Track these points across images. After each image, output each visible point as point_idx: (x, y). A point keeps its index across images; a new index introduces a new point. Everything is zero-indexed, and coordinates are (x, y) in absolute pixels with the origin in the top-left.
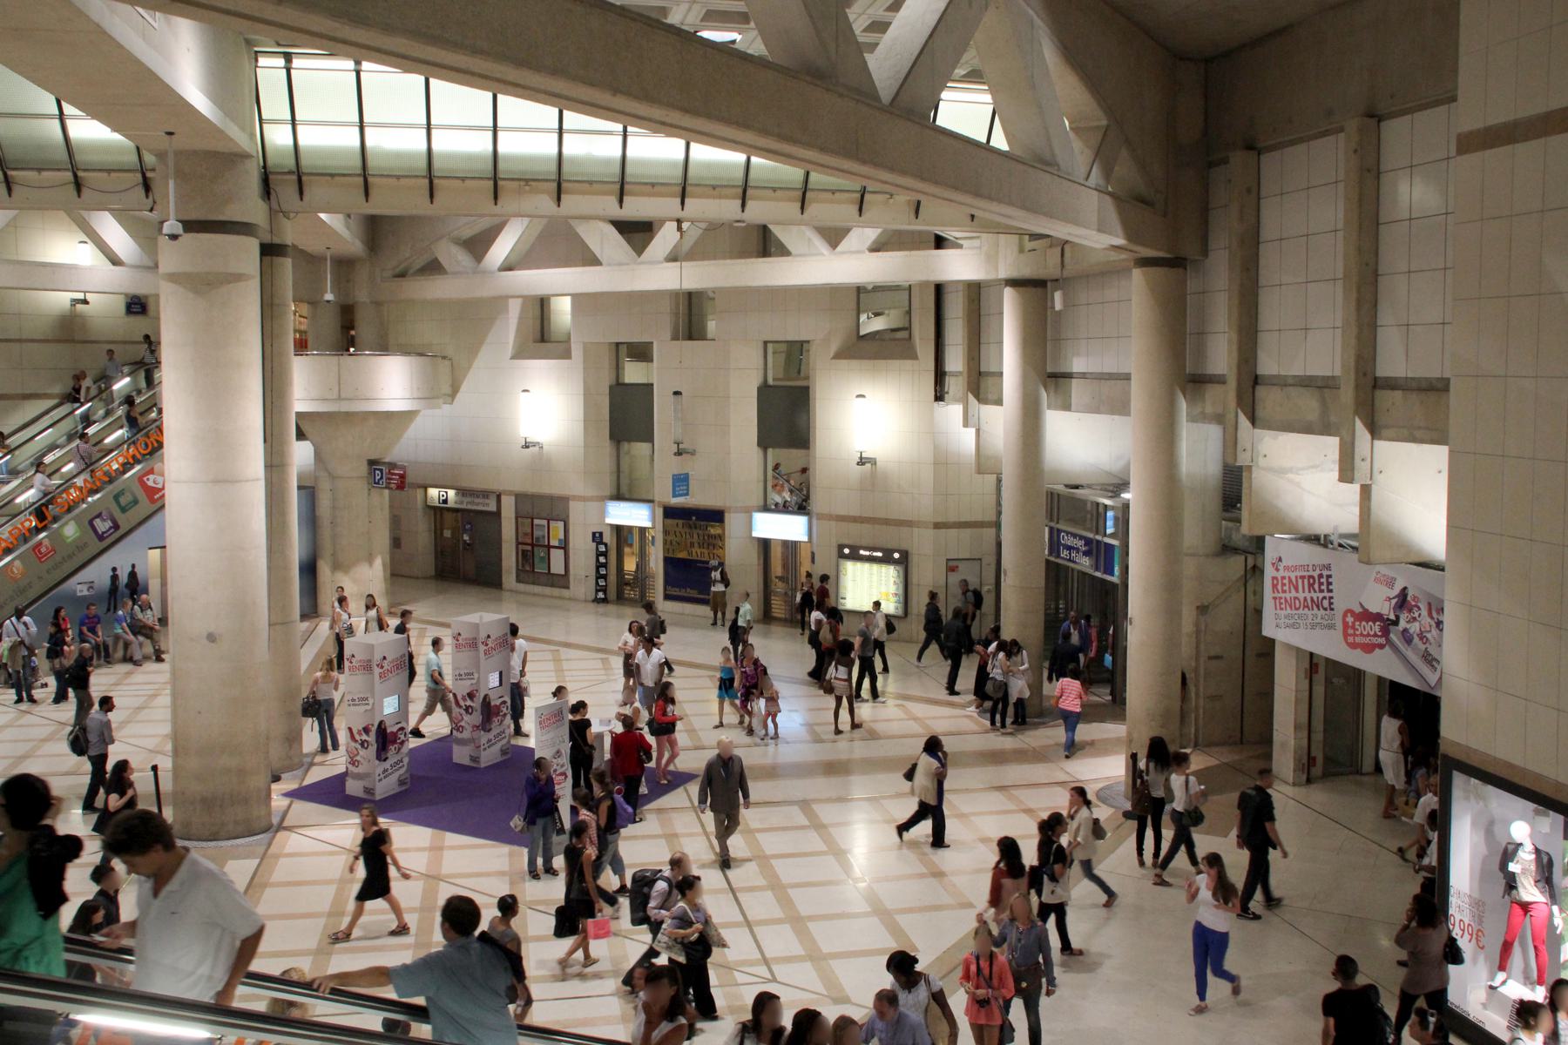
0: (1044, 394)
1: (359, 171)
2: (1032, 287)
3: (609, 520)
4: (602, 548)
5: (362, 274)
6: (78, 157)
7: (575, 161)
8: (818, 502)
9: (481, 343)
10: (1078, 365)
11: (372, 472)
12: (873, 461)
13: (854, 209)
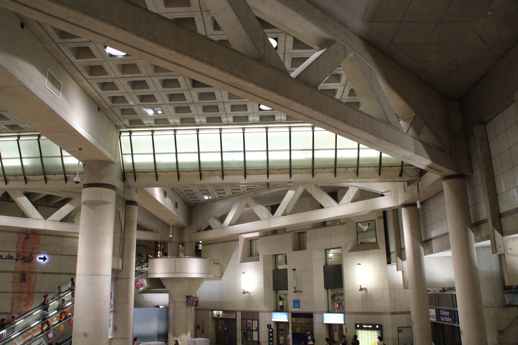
0: (422, 249)
1: (154, 171)
2: (409, 205)
3: (273, 320)
4: (271, 330)
5: (187, 231)
6: (66, 170)
7: (228, 163)
8: (347, 309)
9: (230, 258)
10: (433, 234)
11: (187, 301)
12: (365, 289)
13: (333, 175)
